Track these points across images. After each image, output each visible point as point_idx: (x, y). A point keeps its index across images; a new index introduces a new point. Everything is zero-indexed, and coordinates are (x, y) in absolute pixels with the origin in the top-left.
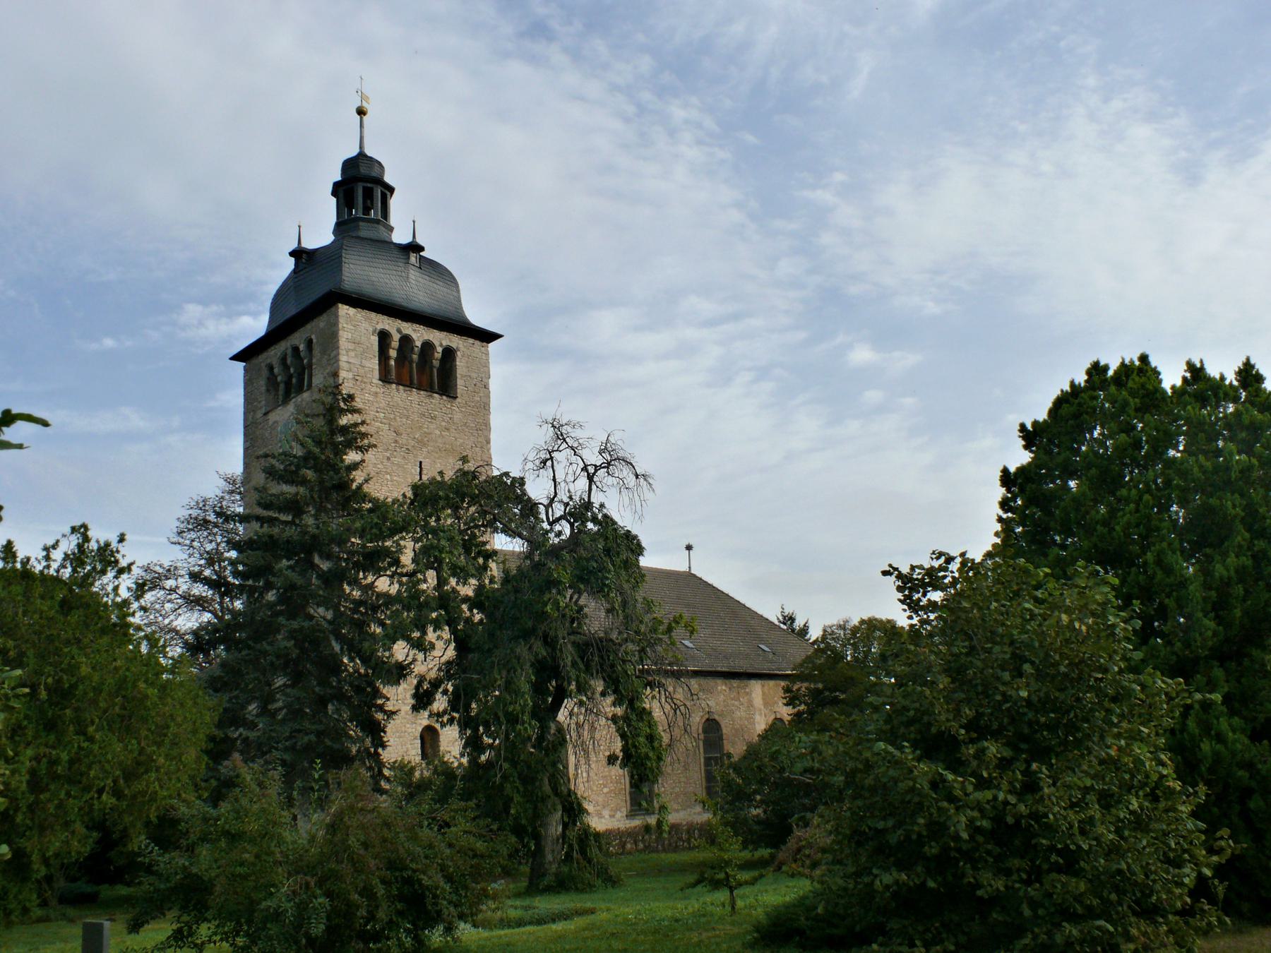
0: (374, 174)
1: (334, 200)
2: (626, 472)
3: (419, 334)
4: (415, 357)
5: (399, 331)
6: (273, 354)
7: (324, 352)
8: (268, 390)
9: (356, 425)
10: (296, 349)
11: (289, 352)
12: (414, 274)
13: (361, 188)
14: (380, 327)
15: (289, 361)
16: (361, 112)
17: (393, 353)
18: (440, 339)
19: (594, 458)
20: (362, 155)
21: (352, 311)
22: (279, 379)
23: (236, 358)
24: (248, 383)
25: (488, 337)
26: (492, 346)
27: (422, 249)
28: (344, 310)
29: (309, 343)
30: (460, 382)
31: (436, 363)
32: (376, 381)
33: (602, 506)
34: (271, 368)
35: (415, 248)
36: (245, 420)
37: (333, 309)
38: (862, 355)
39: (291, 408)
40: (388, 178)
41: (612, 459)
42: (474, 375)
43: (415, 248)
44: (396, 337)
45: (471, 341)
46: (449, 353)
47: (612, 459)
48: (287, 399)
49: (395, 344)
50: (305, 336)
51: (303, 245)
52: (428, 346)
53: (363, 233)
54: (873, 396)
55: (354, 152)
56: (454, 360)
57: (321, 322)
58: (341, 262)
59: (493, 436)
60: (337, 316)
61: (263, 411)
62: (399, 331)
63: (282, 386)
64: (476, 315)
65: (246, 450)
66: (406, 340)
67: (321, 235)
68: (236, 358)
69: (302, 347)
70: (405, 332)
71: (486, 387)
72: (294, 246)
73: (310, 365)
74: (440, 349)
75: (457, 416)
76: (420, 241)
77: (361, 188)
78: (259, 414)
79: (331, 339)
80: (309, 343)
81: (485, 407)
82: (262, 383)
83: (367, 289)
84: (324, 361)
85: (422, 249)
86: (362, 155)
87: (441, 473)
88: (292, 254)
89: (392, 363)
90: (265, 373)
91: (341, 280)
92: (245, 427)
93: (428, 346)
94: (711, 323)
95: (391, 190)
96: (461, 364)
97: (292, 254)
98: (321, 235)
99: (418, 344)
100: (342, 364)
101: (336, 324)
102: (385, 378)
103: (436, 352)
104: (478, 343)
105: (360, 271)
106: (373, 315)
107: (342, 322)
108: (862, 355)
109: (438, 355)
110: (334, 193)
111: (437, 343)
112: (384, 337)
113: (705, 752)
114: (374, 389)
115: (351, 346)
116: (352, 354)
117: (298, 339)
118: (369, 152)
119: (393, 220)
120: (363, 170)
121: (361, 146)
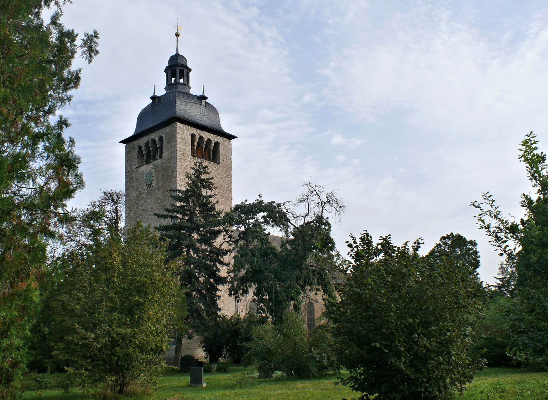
0: (184, 63)
1: (165, 74)
2: (335, 205)
3: (206, 136)
4: (204, 146)
5: (199, 134)
6: (142, 142)
7: (169, 142)
8: (138, 157)
9: (209, 179)
10: (153, 141)
11: (150, 141)
12: (203, 109)
13: (177, 68)
14: (192, 132)
15: (150, 145)
16: (177, 35)
17: (196, 144)
18: (214, 138)
19: (325, 200)
20: (177, 55)
21: (181, 125)
22: (144, 152)
23: (122, 142)
24: (128, 153)
25: (231, 137)
26: (233, 141)
27: (207, 98)
28: (179, 125)
29: (161, 138)
30: (221, 157)
31: (212, 148)
32: (190, 156)
33: (327, 218)
34: (140, 148)
35: (203, 98)
36: (126, 169)
37: (174, 124)
38: (338, 140)
39: (151, 165)
40: (188, 65)
41: (331, 199)
42: (226, 154)
43: (203, 98)
44: (198, 137)
45: (225, 139)
46: (217, 144)
47: (331, 199)
48: (148, 162)
49: (197, 140)
50: (158, 135)
51: (156, 94)
52: (209, 141)
53: (180, 90)
54: (341, 158)
55: (174, 53)
56: (218, 147)
57: (168, 129)
58: (175, 103)
59: (232, 180)
60: (176, 128)
61: (136, 166)
62: (199, 134)
63: (145, 156)
64: (226, 128)
65: (126, 183)
66: (201, 138)
67: (161, 92)
68: (122, 142)
69: (157, 140)
70: (201, 135)
71: (230, 159)
72: (152, 95)
73: (161, 148)
74: (213, 143)
75: (220, 172)
76: (206, 95)
77: (177, 68)
78: (134, 167)
79: (173, 137)
80: (161, 138)
81: (230, 168)
82: (135, 154)
83: (186, 116)
84: (169, 146)
85: (207, 98)
86: (177, 55)
87: (246, 201)
88: (151, 98)
89: (196, 148)
90: (137, 149)
91: (175, 112)
92: (126, 173)
93: (209, 141)
94: (272, 122)
95: (190, 70)
96: (221, 149)
97: (151, 98)
98: (161, 92)
99: (206, 140)
100: (178, 148)
101: (175, 131)
102: (193, 155)
103: (211, 145)
104: (227, 140)
105: (183, 108)
106: (189, 127)
107: (178, 131)
108: (338, 140)
109: (213, 145)
110: (165, 71)
111: (212, 140)
112: (193, 136)
113: (308, 316)
114: (189, 160)
115: (181, 141)
116: (181, 144)
117: (155, 136)
118: (181, 53)
119: (191, 84)
120: (179, 61)
121: (177, 51)
